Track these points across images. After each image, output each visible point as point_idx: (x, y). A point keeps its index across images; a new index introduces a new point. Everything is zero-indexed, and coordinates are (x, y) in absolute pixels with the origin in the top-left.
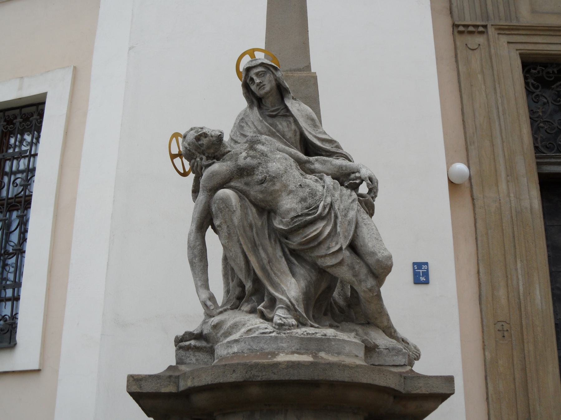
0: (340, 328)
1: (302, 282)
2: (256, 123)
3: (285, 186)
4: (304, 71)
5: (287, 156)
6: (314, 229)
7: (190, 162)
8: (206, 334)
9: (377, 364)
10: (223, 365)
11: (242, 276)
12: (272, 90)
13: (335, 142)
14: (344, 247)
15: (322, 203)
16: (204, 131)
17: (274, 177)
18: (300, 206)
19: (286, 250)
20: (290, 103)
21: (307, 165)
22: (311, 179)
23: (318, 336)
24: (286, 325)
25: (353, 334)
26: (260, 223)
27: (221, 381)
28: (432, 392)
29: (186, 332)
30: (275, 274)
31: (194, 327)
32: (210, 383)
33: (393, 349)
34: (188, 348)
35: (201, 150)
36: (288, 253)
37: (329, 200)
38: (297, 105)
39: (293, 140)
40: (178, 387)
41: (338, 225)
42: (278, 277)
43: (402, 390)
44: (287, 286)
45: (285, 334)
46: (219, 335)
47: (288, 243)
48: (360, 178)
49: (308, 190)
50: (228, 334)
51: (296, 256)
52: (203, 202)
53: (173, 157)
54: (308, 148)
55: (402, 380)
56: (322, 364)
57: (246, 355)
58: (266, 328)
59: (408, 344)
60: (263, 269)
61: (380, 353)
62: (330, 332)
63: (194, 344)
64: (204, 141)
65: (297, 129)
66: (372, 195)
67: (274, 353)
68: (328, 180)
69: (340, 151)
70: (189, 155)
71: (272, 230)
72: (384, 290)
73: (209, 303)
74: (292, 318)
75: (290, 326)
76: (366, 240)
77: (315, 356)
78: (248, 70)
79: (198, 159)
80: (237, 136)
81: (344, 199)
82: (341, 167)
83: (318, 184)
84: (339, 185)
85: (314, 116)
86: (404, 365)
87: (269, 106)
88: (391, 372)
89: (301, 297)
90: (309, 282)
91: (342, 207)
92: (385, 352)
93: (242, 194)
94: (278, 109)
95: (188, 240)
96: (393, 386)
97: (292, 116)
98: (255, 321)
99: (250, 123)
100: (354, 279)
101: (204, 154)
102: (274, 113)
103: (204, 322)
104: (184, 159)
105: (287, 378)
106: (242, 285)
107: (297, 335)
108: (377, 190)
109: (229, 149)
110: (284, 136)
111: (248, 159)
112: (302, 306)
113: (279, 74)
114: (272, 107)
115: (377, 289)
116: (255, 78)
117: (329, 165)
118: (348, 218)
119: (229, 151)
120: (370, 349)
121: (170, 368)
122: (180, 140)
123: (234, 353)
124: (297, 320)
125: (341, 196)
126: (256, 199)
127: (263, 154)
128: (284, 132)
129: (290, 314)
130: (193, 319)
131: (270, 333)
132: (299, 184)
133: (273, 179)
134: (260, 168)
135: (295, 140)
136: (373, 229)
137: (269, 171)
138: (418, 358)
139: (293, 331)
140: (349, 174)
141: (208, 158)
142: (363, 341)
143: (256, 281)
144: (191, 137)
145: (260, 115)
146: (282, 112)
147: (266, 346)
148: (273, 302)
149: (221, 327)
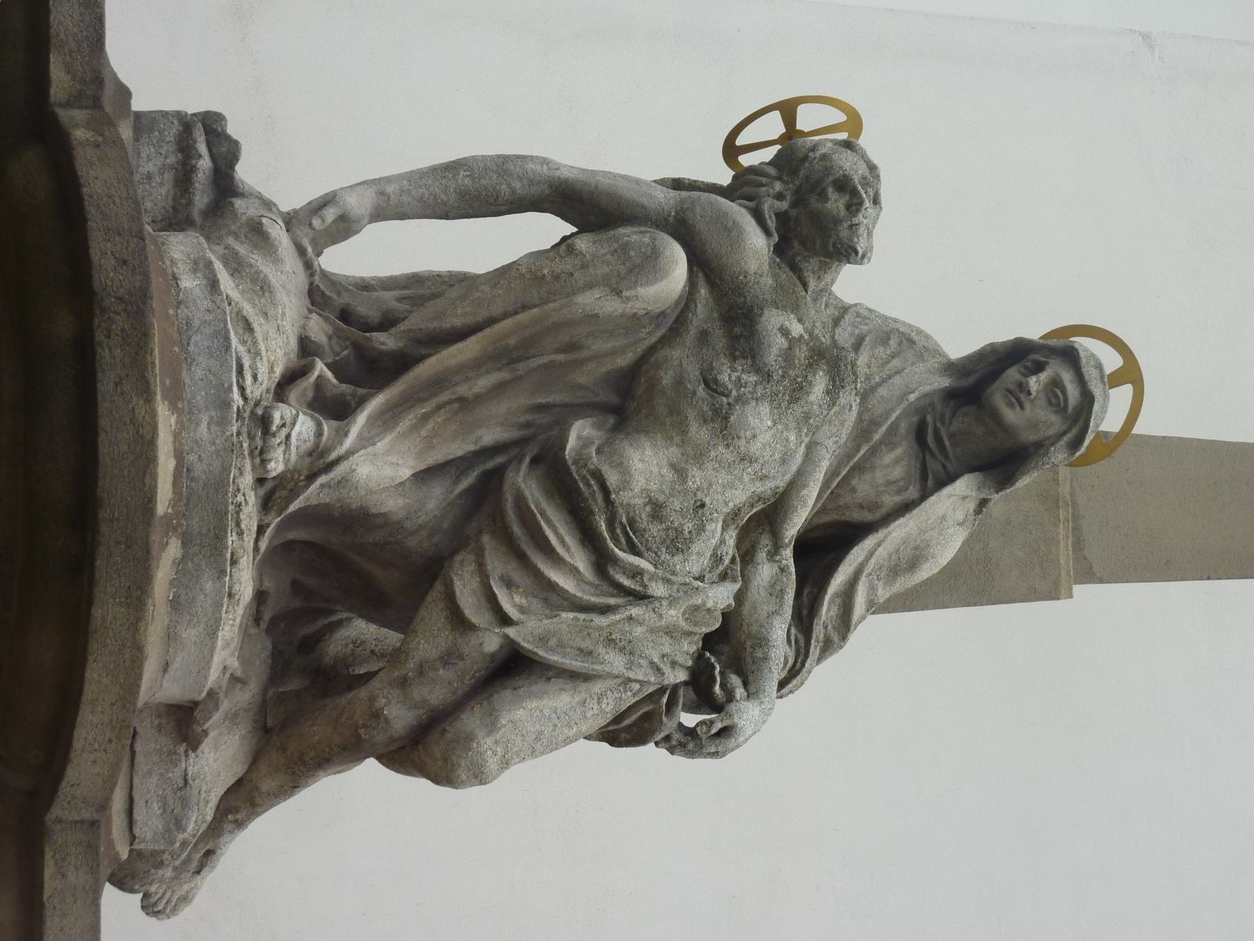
0: (253, 631)
1: (401, 502)
2: (897, 380)
3: (699, 457)
4: (1076, 560)
5: (794, 467)
6: (568, 539)
7: (770, 163)
8: (232, 204)
9: (138, 747)
10: (141, 231)
11: (418, 321)
12: (1003, 421)
13: (844, 638)
14: (511, 631)
15: (651, 568)
16: (867, 204)
17: (726, 418)
18: (639, 501)
19: (500, 459)
20: (964, 486)
21: (765, 542)
22: (722, 542)
23: (231, 539)
24: (264, 441)
25: (236, 664)
26: (582, 379)
27: (91, 224)
28: (48, 912)
29: (236, 143)
30: (425, 418)
31: (246, 172)
32: (85, 190)
33: (185, 803)
34: (185, 148)
35: (809, 197)
36: (490, 464)
37: (658, 589)
38: (960, 516)
39: (846, 499)
40: (68, 105)
41: (582, 616)
42: (415, 428)
43: (56, 811)
44: (388, 452)
45: (239, 434)
46: (230, 241)
47: (520, 462)
48: (730, 697)
49: (688, 526)
50: (236, 266)
51: (481, 501)
52: (645, 201)
53: (788, 110)
54: (822, 550)
55: (87, 815)
56: (147, 536)
57: (171, 312)
58: (255, 377)
59: (198, 872)
60: (439, 383)
61: (171, 758)
62: (245, 581)
63: (203, 159)
64: (836, 203)
65: (883, 511)
66: (677, 737)
67: (180, 398)
68: (721, 596)
69: (814, 651)
70: (794, 156)
71: (564, 415)
72: (371, 763)
73: (330, 214)
74: (286, 461)
75: (261, 453)
76: (533, 704)
77: (170, 526)
78: (1070, 356)
79: (778, 186)
80: (854, 325)
81: (657, 644)
82: (762, 642)
83: (706, 561)
84: (705, 630)
85: (926, 571)
86: (133, 838)
87: (956, 426)
88: (110, 783)
89: (354, 500)
90: (399, 526)
91: (638, 631)
92: (176, 775)
93: (676, 322)
94: (945, 455)
95: (524, 157)
96: (71, 774)
97: (924, 496)
98: (274, 350)
99: (896, 363)
100: (411, 664)
101: (794, 205)
102: (930, 439)
103: (268, 205)
104: (778, 147)
105: (103, 422)
106: (388, 322)
107: (234, 472)
108: (691, 754)
109: (812, 284)
110: (859, 469)
111: (781, 342)
112: (325, 498)
113: (1058, 455)
114: (952, 436)
115: (380, 738)
116: (1044, 376)
117: (764, 609)
118: (601, 650)
119: (805, 286)
120: (184, 721)
121: (124, 94)
122: (843, 136)
123: (175, 278)
124: (281, 478)
125: (670, 632)
126: (658, 366)
127: (798, 391)
128: (873, 468)
129: (300, 457)
130: (277, 174)
131: (242, 389)
132: (707, 501)
133: (721, 420)
134: (753, 378)
135: (847, 507)
136: (569, 726)
137: (743, 403)
138: (149, 907)
139: (248, 461)
140: (740, 672)
141: (782, 217)
142: (211, 693)
143: (401, 363)
144: (846, 162)
145: (925, 395)
146: (934, 466)
147: (199, 373)
148: (335, 409)
149: (255, 246)
